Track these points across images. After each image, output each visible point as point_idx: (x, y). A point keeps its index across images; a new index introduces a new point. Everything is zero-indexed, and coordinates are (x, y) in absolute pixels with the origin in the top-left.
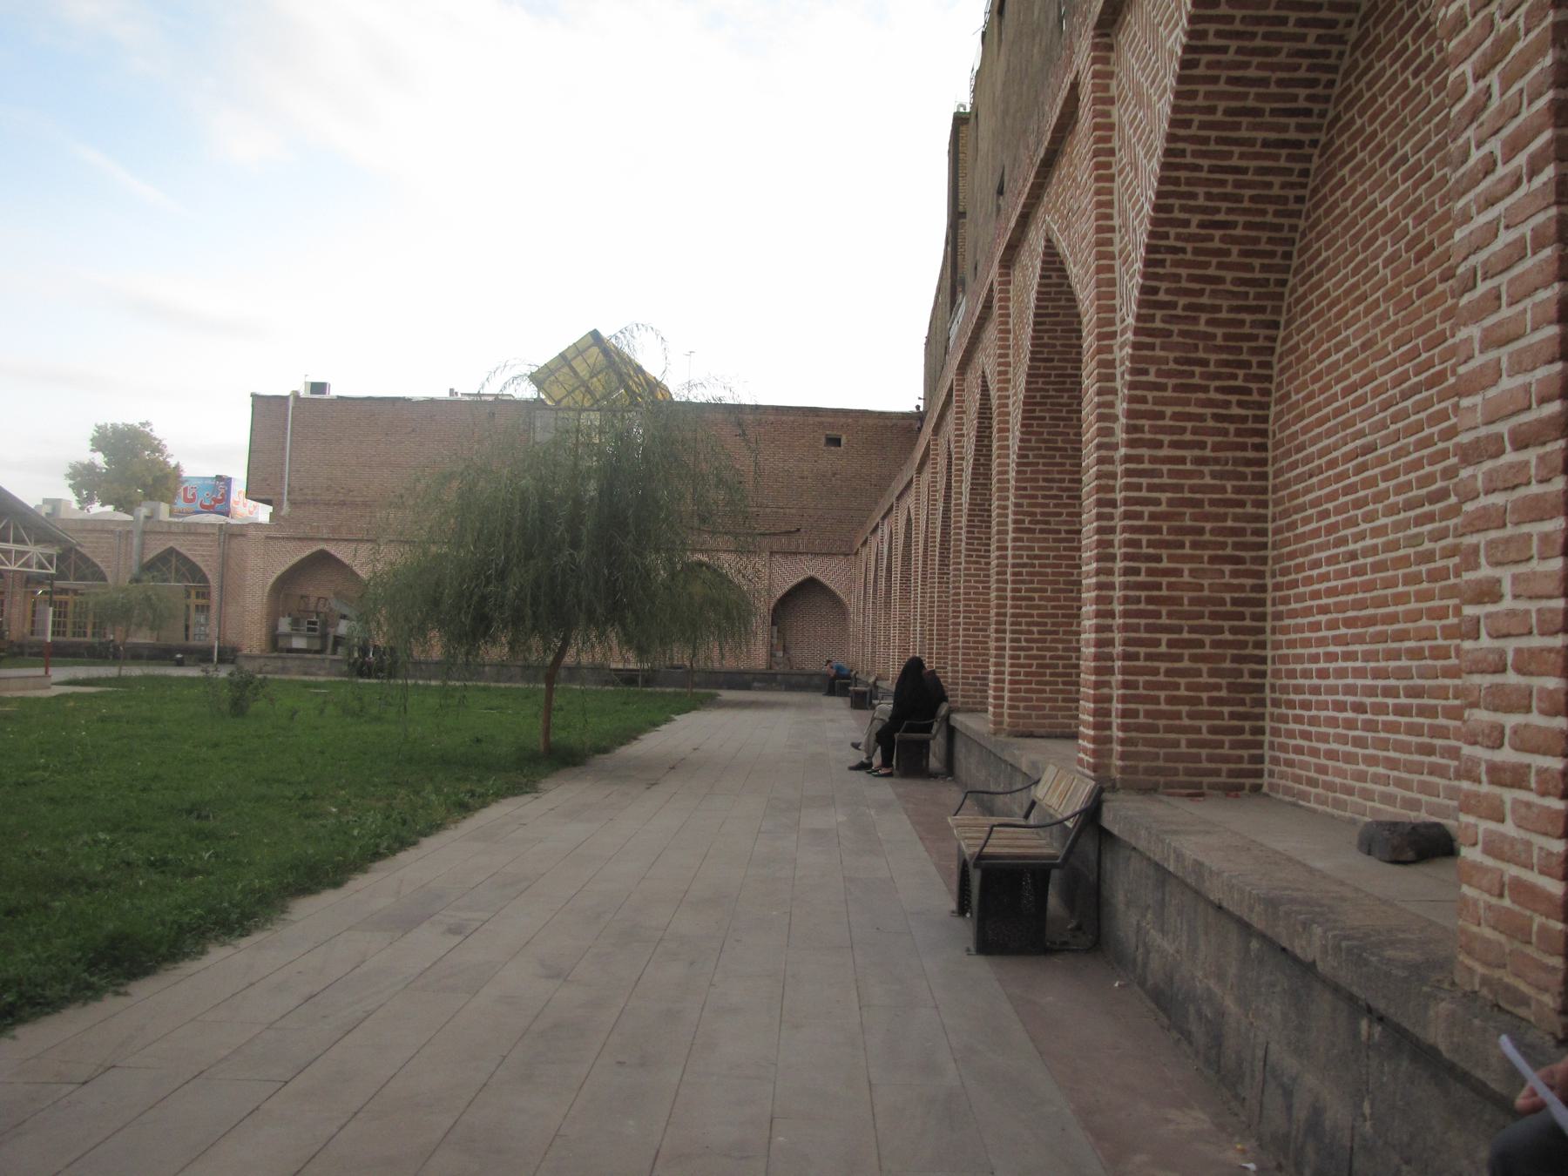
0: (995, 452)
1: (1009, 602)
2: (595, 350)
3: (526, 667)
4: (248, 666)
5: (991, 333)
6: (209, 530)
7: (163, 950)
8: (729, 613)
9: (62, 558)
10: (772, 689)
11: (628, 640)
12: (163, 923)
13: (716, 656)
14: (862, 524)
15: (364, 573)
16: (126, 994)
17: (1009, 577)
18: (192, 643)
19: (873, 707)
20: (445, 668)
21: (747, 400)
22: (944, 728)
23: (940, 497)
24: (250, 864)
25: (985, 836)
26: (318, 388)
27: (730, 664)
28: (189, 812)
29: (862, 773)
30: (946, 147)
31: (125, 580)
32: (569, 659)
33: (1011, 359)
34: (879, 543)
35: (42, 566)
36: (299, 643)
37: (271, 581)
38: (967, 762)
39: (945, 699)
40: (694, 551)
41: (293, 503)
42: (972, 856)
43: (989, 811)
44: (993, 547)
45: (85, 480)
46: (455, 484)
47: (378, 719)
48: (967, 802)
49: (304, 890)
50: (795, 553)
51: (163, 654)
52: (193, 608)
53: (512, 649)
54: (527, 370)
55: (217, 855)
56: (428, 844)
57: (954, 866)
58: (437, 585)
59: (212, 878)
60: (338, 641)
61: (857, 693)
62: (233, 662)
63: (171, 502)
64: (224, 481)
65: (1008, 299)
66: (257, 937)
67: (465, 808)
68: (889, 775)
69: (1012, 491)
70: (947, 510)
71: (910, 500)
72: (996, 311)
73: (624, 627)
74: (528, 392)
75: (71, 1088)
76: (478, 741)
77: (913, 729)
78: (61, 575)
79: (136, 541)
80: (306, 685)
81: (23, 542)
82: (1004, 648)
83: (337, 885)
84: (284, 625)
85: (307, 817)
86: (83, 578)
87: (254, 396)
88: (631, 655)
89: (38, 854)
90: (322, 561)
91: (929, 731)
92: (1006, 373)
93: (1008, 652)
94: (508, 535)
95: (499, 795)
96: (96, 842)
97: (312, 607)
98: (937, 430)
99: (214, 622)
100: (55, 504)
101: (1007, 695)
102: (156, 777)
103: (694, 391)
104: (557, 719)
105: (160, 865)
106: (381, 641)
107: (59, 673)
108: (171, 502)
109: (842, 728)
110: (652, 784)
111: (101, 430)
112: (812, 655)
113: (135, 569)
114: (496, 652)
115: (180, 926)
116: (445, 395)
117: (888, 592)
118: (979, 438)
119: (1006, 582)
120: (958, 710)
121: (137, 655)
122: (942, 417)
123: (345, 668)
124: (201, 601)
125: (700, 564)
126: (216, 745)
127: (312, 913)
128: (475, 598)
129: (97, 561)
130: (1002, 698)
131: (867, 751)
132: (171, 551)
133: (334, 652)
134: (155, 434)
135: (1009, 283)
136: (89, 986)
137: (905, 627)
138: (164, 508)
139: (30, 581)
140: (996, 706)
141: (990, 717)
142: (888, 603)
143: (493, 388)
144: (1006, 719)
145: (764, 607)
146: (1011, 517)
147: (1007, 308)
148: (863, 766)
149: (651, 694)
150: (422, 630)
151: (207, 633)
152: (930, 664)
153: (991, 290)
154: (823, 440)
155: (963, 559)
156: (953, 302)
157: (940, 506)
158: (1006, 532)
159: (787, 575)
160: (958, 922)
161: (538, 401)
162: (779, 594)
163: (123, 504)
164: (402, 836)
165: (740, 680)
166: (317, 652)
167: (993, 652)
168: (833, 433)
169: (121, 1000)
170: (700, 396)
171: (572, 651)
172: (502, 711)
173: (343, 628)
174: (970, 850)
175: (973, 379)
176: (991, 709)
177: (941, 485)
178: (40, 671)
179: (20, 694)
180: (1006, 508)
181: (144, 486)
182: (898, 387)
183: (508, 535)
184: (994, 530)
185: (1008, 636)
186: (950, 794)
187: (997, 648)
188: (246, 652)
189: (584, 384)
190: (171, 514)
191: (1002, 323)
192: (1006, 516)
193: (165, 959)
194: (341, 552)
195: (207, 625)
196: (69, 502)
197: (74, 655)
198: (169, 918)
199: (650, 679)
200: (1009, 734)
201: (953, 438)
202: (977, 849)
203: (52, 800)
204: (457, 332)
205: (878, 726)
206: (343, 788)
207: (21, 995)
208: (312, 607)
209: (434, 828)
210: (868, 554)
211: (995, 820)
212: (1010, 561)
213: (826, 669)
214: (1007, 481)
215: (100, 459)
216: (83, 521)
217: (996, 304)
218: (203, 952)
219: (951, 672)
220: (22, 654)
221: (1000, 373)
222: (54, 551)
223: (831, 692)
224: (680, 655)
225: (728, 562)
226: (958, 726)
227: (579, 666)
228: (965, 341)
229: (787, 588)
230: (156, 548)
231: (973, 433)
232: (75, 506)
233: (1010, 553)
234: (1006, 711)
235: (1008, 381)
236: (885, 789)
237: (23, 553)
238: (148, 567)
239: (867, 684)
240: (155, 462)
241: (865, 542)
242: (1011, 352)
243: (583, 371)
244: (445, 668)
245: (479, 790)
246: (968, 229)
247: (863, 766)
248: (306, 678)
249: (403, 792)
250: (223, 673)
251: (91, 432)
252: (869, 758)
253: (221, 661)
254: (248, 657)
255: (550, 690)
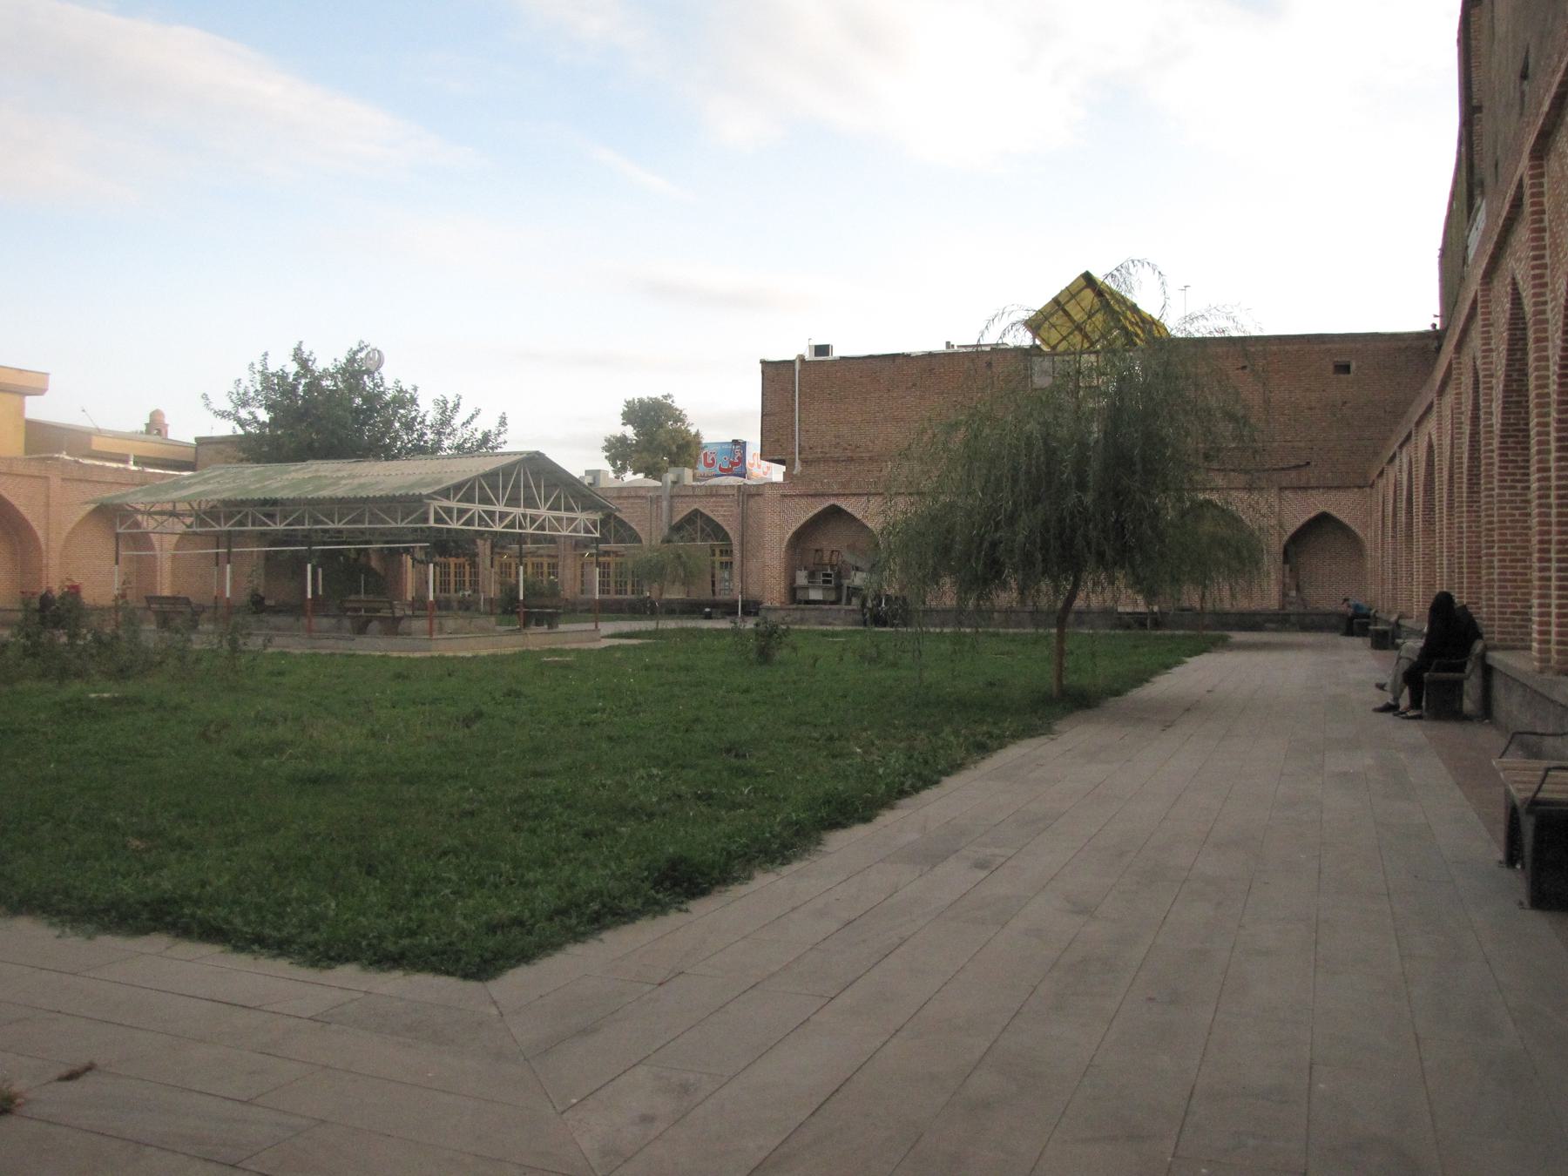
0: (1532, 363)
1: (1554, 528)
2: (1088, 295)
3: (1036, 612)
4: (772, 617)
5: (1523, 234)
6: (730, 492)
7: (716, 874)
8: (1239, 554)
9: (604, 523)
10: (1287, 630)
11: (1138, 583)
12: (714, 849)
13: (1225, 596)
14: (1376, 454)
15: (875, 524)
16: (687, 911)
17: (1553, 500)
18: (719, 597)
19: (1397, 647)
20: (958, 616)
21: (1255, 332)
22: (1479, 672)
23: (1466, 419)
24: (785, 799)
25: (1538, 780)
26: (822, 350)
27: (1243, 604)
28: (728, 751)
29: (1390, 715)
30: (1455, 36)
31: (657, 540)
32: (1079, 603)
33: (1547, 260)
34: (1397, 473)
35: (588, 531)
36: (815, 595)
37: (788, 536)
38: (1508, 703)
39: (1479, 636)
40: (1204, 490)
41: (804, 462)
42: (1524, 801)
43: (1536, 754)
44: (1533, 468)
45: (618, 451)
46: (961, 434)
47: (894, 665)
48: (1512, 747)
49: (835, 825)
50: (1305, 488)
51: (692, 609)
52: (717, 565)
53: (1021, 593)
54: (1025, 316)
55: (755, 790)
56: (949, 783)
57: (1501, 815)
58: (948, 532)
59: (753, 812)
60: (855, 591)
61: (1377, 631)
62: (756, 614)
63: (694, 467)
64: (739, 445)
65: (1541, 194)
66: (797, 865)
67: (983, 749)
68: (1419, 717)
69: (1554, 406)
70: (1474, 435)
71: (1431, 425)
72: (1527, 208)
73: (1132, 567)
74: (1025, 339)
75: (648, 988)
76: (991, 684)
77: (1444, 667)
78: (604, 539)
79: (665, 504)
80: (824, 634)
81: (572, 510)
82: (1549, 579)
83: (867, 820)
84: (802, 578)
85: (834, 757)
86: (622, 541)
87: (764, 363)
88: (1140, 598)
89: (604, 786)
90: (834, 513)
91: (1462, 671)
92: (1542, 276)
93: (1554, 583)
94: (1015, 481)
95: (1017, 736)
96: (651, 776)
97: (826, 560)
98: (1459, 347)
99: (737, 580)
100: (595, 474)
101: (1554, 629)
102: (697, 720)
103: (1196, 324)
104: (1069, 663)
105: (707, 798)
106: (891, 592)
107: (607, 627)
108: (694, 467)
109: (1363, 670)
110: (1167, 726)
111: (629, 404)
112: (1328, 595)
113: (666, 530)
114: (1006, 598)
115: (729, 853)
116: (941, 348)
117: (1410, 524)
118: (1511, 351)
119: (1549, 506)
120: (1495, 648)
121: (671, 610)
122: (1465, 332)
123: (859, 617)
124: (725, 559)
125: (1209, 502)
126: (747, 691)
127: (844, 844)
128: (986, 545)
129: (633, 525)
130: (1548, 633)
131: (1393, 691)
132: (696, 513)
133: (849, 602)
134: (677, 405)
135: (1542, 175)
136: (657, 902)
137: (1430, 562)
138: (688, 472)
139: (579, 544)
140: (1541, 642)
141: (1535, 654)
142: (1409, 536)
143: (991, 338)
144: (1554, 656)
145: (1275, 544)
146: (1553, 435)
147: (1541, 204)
148: (1390, 708)
149: (1158, 638)
150: (935, 577)
151: (731, 589)
152: (1461, 598)
153: (1520, 185)
154: (1331, 367)
155: (1496, 484)
156: (1471, 208)
157: (1467, 429)
158: (1548, 452)
159: (1298, 511)
160: (1507, 873)
161: (1035, 347)
162: (1291, 530)
163: (652, 471)
164: (924, 777)
165: (1251, 622)
166: (832, 603)
167: (1536, 583)
168: (1343, 359)
169: (683, 915)
170: (1200, 330)
171: (1082, 595)
172: (1016, 659)
173: (858, 579)
174: (1520, 795)
175: (1501, 288)
176: (1535, 645)
177: (1467, 407)
178: (591, 626)
179: (574, 646)
180: (1547, 425)
181: (669, 454)
182: (1412, 305)
183: (1015, 481)
184: (1534, 449)
185: (1554, 565)
186: (1485, 737)
187: (1541, 579)
188: (768, 604)
189: (1079, 328)
190: (695, 478)
191: (1534, 222)
192: (1548, 434)
193: (718, 883)
194: (843, 504)
195: (730, 580)
196: (606, 473)
197: (620, 611)
198: (719, 846)
199: (1158, 622)
200: (1559, 673)
201: (1479, 354)
202: (1530, 794)
203: (610, 739)
204: (953, 286)
205: (1405, 665)
206: (865, 730)
207: (604, 905)
208: (826, 560)
209: (955, 767)
210: (1386, 486)
211: (1545, 763)
212: (1554, 483)
213: (1343, 608)
214: (1548, 395)
215: (630, 432)
216: (620, 489)
217: (1527, 200)
218: (750, 878)
219: (1487, 610)
220: (574, 611)
221: (1535, 277)
222: (597, 516)
223: (1349, 632)
224: (1191, 597)
225: (1238, 502)
226: (1496, 665)
227: (1089, 611)
228: (1490, 248)
229: (1298, 524)
230: (683, 510)
231: (1503, 347)
232: (612, 475)
233: (1553, 474)
234: (1554, 647)
235: (1545, 285)
236: (1414, 732)
237: (573, 520)
238: (677, 528)
239: (1389, 623)
240: (678, 431)
241: (1381, 474)
242: (1547, 252)
243: (1078, 316)
244: (958, 616)
245: (996, 731)
246: (1485, 123)
247: (1390, 708)
248: (824, 628)
249: (923, 734)
250: (750, 624)
251: (621, 408)
252: (1396, 699)
253: (746, 613)
254: (769, 609)
255: (1061, 637)
